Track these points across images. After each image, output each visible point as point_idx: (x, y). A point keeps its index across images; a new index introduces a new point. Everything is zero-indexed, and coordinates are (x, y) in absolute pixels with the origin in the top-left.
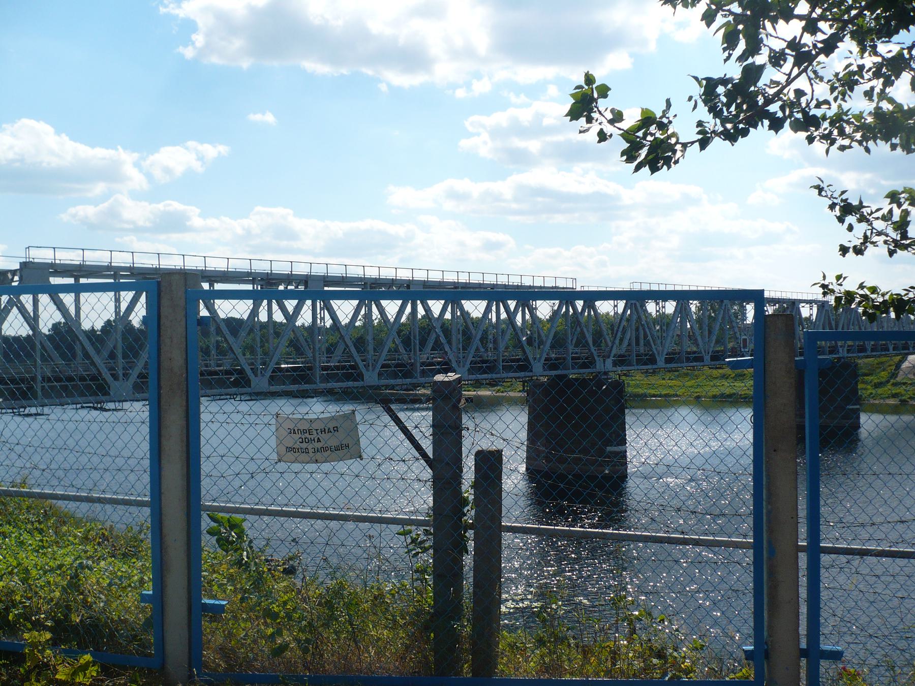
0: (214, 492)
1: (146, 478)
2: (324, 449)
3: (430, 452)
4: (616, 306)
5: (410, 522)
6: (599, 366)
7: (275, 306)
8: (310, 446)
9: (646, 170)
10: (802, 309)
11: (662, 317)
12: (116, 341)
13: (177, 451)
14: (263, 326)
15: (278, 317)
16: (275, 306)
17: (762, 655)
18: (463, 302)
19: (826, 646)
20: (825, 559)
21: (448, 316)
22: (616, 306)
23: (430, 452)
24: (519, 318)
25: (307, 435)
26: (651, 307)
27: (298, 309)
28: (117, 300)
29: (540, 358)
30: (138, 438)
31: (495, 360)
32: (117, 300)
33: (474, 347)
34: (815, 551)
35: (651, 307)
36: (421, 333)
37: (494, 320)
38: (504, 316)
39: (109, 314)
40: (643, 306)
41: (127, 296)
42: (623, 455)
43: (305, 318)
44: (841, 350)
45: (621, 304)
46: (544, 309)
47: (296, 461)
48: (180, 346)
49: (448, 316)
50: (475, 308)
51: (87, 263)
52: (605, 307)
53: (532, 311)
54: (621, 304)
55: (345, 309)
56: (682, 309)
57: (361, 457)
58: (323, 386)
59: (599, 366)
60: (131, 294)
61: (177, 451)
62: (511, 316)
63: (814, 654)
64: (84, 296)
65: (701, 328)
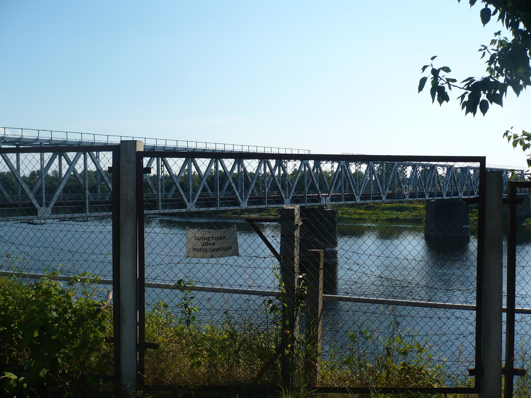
0: (153, 275)
1: (110, 267)
2: (218, 250)
3: (278, 251)
4: (332, 167)
5: (271, 294)
6: (323, 202)
7: (89, 160)
8: (208, 247)
9: (493, 107)
10: (438, 170)
11: (358, 174)
12: (42, 183)
13: (128, 251)
14: (166, 177)
15: (92, 167)
16: (89, 160)
17: (478, 372)
18: (196, 159)
19: (517, 366)
20: (517, 316)
21: (236, 171)
22: (332, 167)
23: (278, 251)
24: (277, 172)
25: (206, 241)
26: (353, 168)
27: (76, 159)
28: (42, 159)
29: (289, 196)
30: (105, 242)
31: (263, 197)
32: (42, 159)
33: (251, 189)
34: (511, 311)
35: (353, 168)
36: (216, 180)
37: (263, 172)
38: (268, 170)
39: (38, 167)
40: (348, 166)
41: (48, 156)
42: (335, 253)
43: (79, 168)
44: (460, 193)
45: (336, 165)
46: (291, 166)
47: (194, 257)
48: (130, 189)
49: (236, 171)
50: (251, 166)
51: (24, 137)
52: (326, 167)
53: (243, 166)
54: (336, 165)
55: (176, 164)
56: (370, 169)
57: (238, 255)
58: (162, 211)
59: (323, 202)
60: (148, 159)
61: (128, 251)
62: (272, 171)
63: (510, 372)
64: (22, 156)
65: (381, 181)
